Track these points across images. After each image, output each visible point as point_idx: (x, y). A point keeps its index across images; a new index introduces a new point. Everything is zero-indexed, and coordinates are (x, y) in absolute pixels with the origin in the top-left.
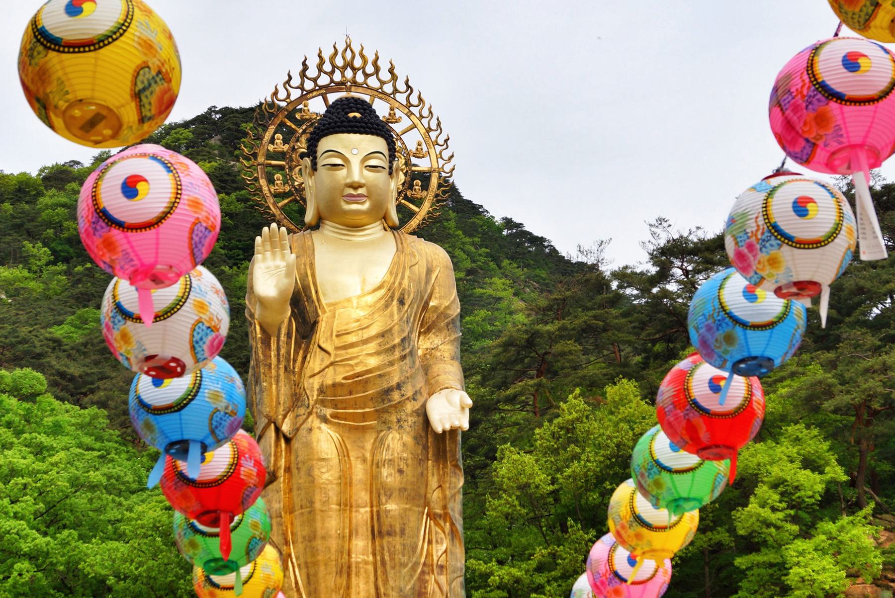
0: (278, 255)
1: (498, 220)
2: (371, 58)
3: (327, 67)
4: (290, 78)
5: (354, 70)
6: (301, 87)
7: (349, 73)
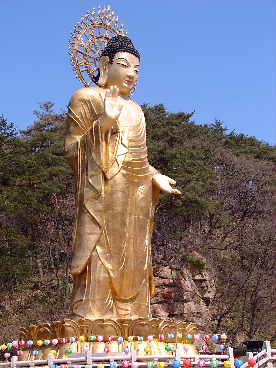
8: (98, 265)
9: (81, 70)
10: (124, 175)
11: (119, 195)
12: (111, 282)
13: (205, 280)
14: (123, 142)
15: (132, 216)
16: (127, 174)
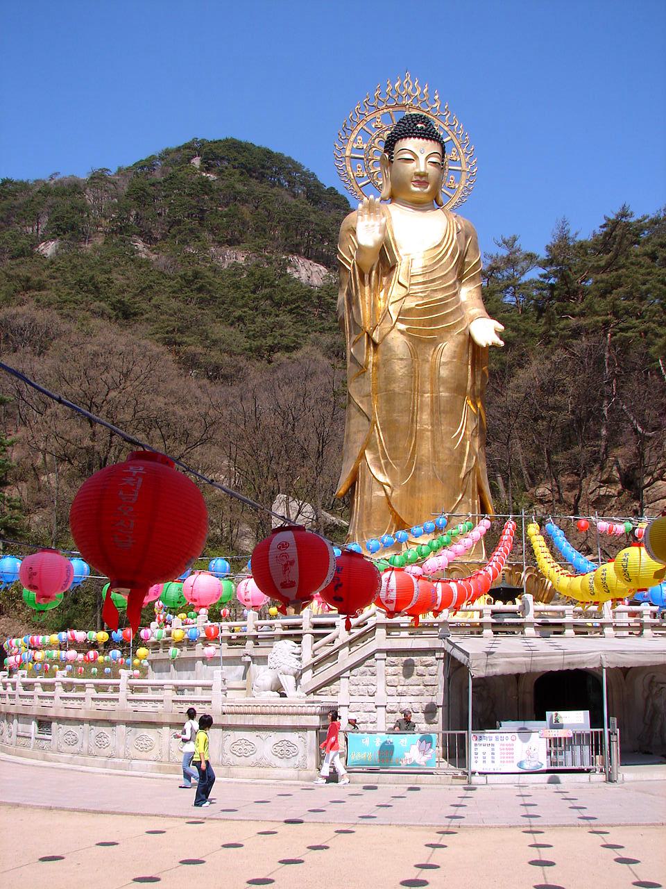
8: (367, 480)
9: (359, 185)
10: (402, 332)
11: (399, 368)
12: (389, 503)
14: (400, 281)
15: (426, 395)
16: (407, 329)
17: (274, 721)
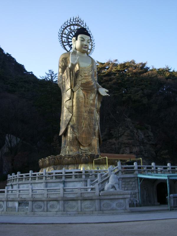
0: (75, 56)
1: (6, 53)
2: (82, 21)
3: (75, 20)
4: (68, 21)
5: (79, 22)
6: (70, 23)
7: (78, 23)
13: (150, 136)
17: (116, 197)
